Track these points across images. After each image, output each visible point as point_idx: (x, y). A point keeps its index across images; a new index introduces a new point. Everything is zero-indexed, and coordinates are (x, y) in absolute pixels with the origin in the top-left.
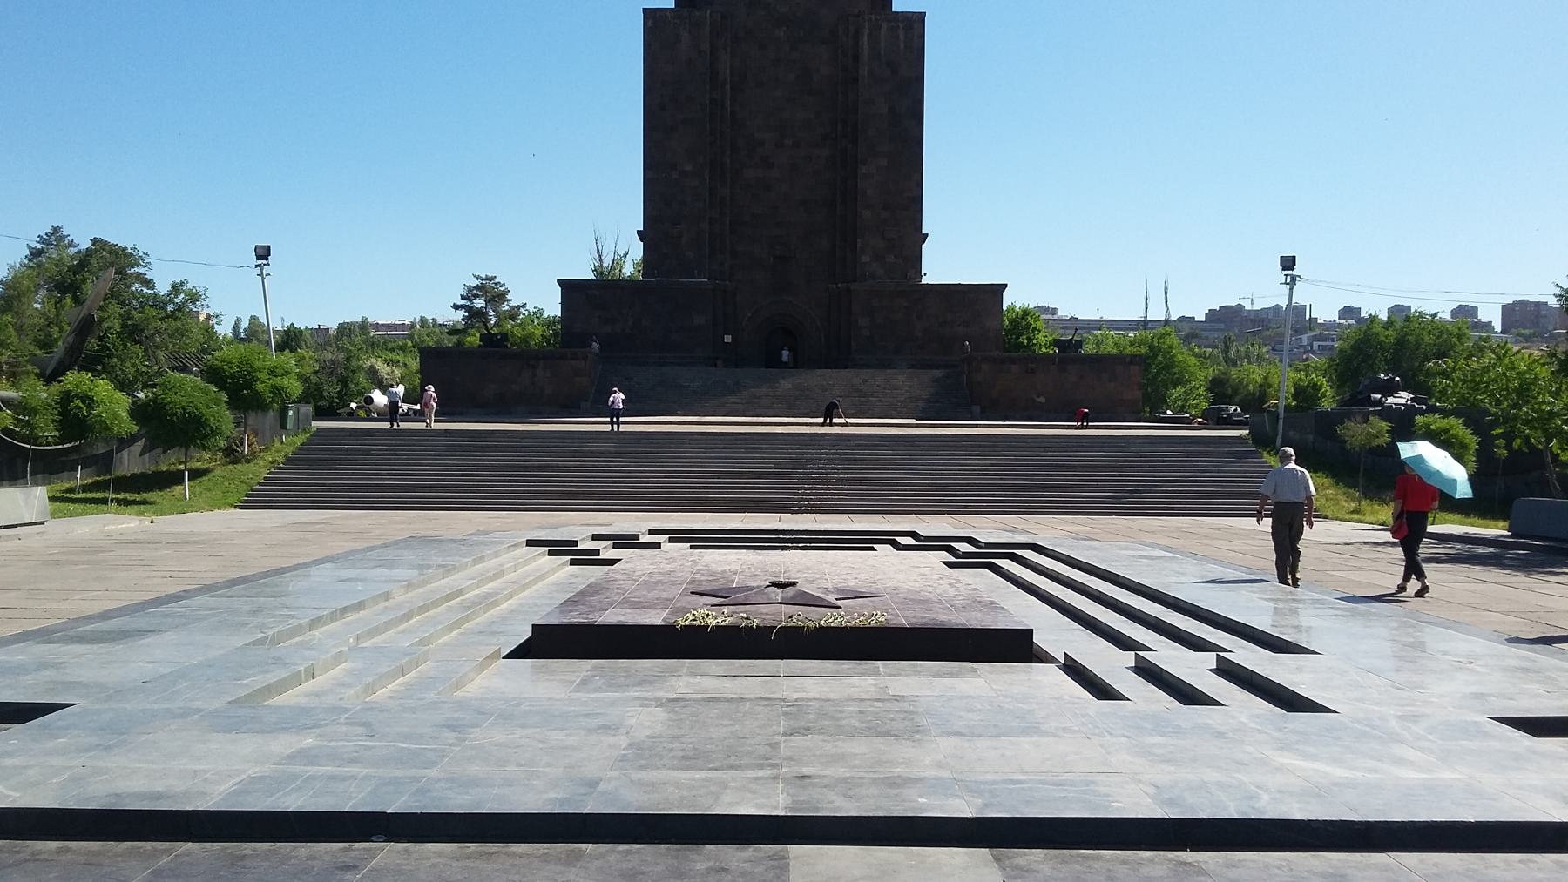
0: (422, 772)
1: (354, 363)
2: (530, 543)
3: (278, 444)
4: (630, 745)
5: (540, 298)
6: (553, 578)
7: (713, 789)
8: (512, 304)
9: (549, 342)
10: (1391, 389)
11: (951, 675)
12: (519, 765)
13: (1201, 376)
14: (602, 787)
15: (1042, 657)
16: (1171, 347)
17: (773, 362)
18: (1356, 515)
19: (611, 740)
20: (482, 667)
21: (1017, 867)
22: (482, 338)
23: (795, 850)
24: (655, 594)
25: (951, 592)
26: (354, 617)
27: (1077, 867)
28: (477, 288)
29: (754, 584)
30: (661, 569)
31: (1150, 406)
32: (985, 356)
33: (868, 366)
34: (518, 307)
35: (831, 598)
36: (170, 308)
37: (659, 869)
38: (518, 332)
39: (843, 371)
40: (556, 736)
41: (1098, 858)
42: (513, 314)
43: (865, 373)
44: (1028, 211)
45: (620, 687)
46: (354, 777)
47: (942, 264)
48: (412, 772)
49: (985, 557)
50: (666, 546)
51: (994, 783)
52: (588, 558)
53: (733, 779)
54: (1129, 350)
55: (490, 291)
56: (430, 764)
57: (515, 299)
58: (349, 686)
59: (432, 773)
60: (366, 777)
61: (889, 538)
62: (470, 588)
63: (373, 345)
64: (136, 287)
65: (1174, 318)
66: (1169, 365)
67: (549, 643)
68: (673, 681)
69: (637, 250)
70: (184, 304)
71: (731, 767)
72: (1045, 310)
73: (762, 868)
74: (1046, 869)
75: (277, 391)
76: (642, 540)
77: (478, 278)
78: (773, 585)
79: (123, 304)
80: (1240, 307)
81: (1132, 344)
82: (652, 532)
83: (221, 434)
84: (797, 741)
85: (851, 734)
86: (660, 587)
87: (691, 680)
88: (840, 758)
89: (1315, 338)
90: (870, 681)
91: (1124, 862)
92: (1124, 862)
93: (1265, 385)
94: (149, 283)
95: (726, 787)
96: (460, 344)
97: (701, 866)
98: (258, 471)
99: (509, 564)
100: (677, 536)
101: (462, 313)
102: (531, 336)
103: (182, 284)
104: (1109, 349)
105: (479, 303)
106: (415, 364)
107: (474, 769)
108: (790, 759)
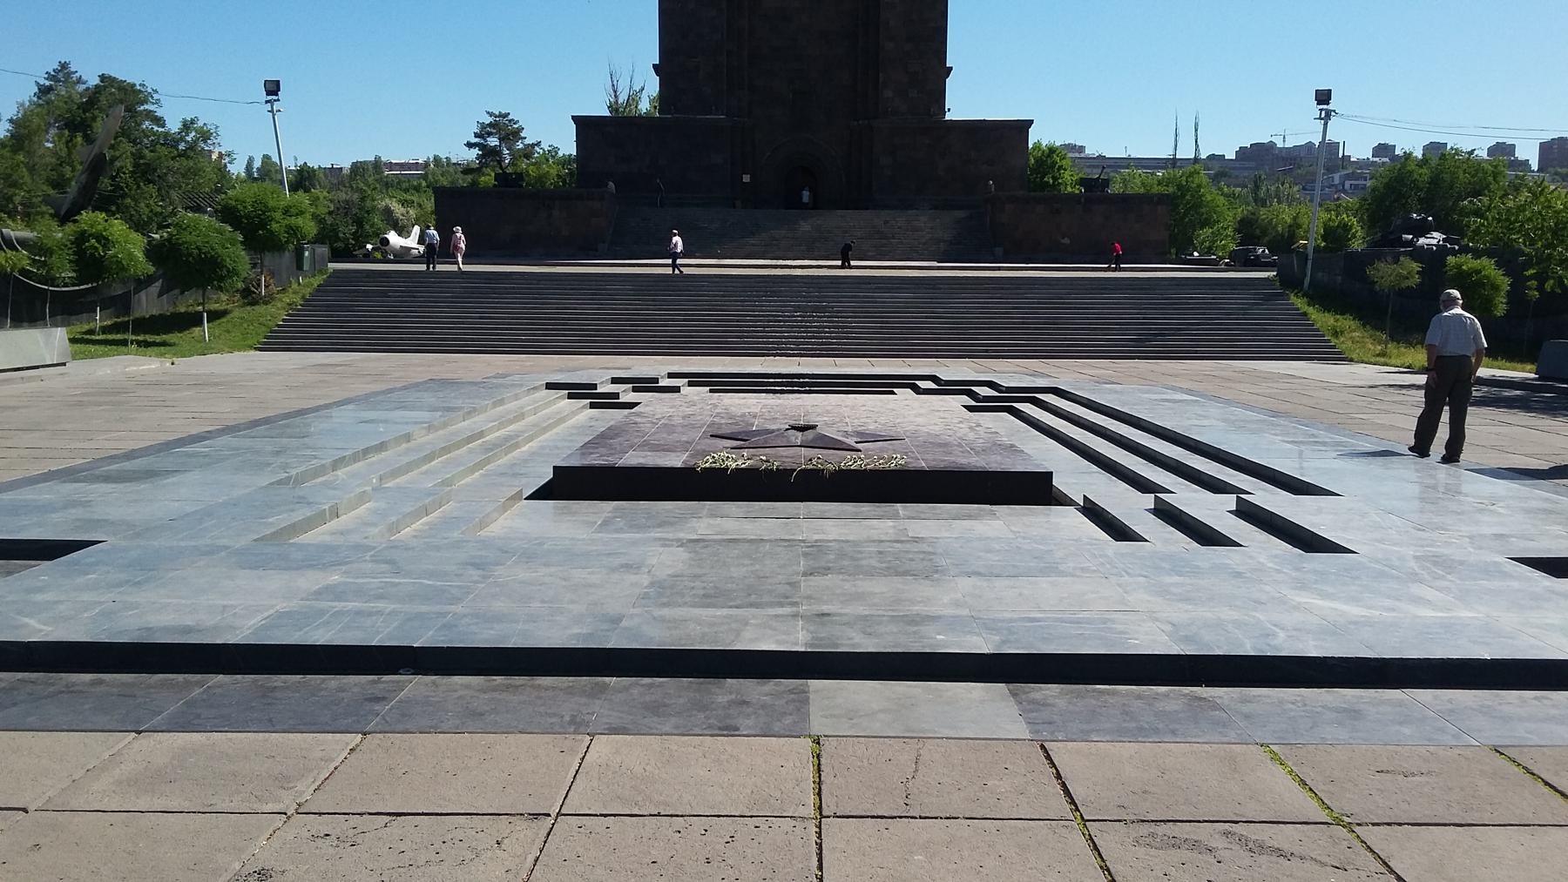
1: (368, 203)
2: (550, 386)
3: (295, 286)
4: (652, 584)
7: (734, 626)
8: (527, 142)
9: (564, 182)
10: (1423, 230)
11: (970, 517)
12: (543, 601)
13: (1230, 217)
14: (624, 623)
15: (1061, 500)
16: (1199, 186)
18: (1381, 358)
19: (633, 578)
21: (1033, 702)
25: (971, 436)
26: (375, 458)
28: (490, 125)
30: (682, 413)
31: (1176, 247)
34: (533, 145)
35: (851, 441)
36: (182, 146)
37: (681, 701)
38: (532, 171)
39: (867, 214)
41: (1114, 693)
42: (528, 152)
47: (969, 98)
48: (437, 608)
49: (1005, 401)
50: (686, 390)
51: (1011, 620)
53: (754, 617)
54: (1156, 189)
55: (503, 128)
56: (456, 600)
57: (530, 136)
58: (375, 525)
59: (458, 608)
61: (909, 382)
62: (491, 430)
63: (387, 185)
64: (147, 124)
65: (1203, 156)
66: (1198, 204)
67: (569, 485)
68: (694, 523)
69: (653, 86)
70: (195, 142)
71: (751, 605)
73: (782, 702)
74: (1061, 703)
75: (293, 231)
77: (491, 114)
78: (793, 428)
79: (134, 142)
80: (1272, 145)
82: (671, 375)
83: (237, 274)
84: (816, 581)
85: (871, 573)
87: (711, 521)
88: (859, 597)
89: (1348, 177)
90: (890, 523)
91: (1139, 697)
92: (1139, 697)
93: (1295, 225)
94: (159, 121)
95: (747, 624)
96: (474, 183)
97: (722, 699)
98: (276, 313)
99: (531, 408)
100: (696, 379)
101: (476, 151)
103: (192, 122)
104: (1136, 188)
105: (493, 141)
106: (430, 205)
107: (500, 605)
108: (809, 597)
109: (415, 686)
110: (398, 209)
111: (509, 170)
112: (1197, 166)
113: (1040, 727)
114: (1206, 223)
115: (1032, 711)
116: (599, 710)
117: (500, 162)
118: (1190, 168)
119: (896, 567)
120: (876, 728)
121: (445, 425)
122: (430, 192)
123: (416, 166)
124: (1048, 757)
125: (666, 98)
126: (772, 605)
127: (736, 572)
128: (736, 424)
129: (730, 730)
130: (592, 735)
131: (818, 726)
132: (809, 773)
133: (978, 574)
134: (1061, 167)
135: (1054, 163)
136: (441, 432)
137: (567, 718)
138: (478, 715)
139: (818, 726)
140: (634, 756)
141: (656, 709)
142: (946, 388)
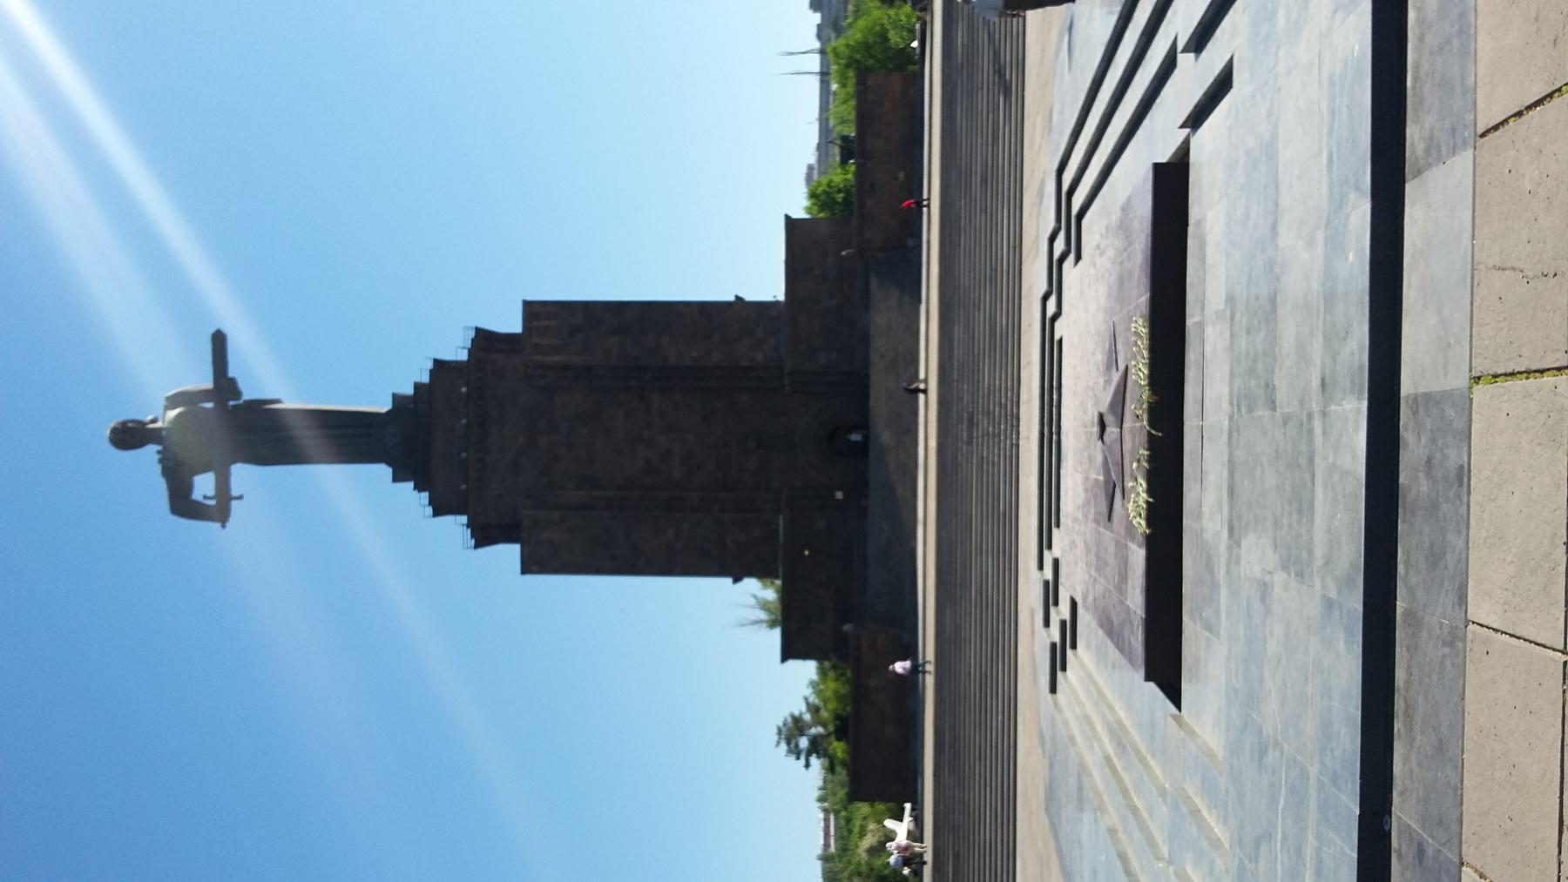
0: (1313, 781)
1: (864, 869)
2: (1053, 689)
4: (1285, 568)
5: (799, 684)
6: (1091, 666)
7: (1336, 478)
11: (1202, 246)
12: (1306, 682)
14: (1333, 594)
15: (1184, 152)
16: (848, 46)
17: (862, 450)
19: (1278, 590)
20: (1191, 732)
21: (1428, 151)
22: (839, 739)
23: (1406, 387)
24: (1111, 560)
25: (1111, 253)
26: (1135, 865)
27: (1426, 88)
28: (788, 744)
29: (1100, 458)
30: (1080, 552)
31: (909, 66)
32: (858, 234)
33: (867, 351)
34: (808, 704)
35: (1116, 377)
37: (1427, 530)
38: (832, 705)
40: (1273, 646)
41: (1417, 67)
42: (814, 709)
43: (874, 357)
44: (717, 213)
45: (1215, 587)
46: (1318, 851)
47: (766, 283)
48: (1313, 792)
49: (1070, 223)
50: (1057, 551)
51: (1331, 184)
52: (1070, 632)
53: (1325, 458)
54: (851, 89)
55: (792, 731)
56: (1304, 775)
57: (799, 708)
58: (1212, 863)
59: (1314, 770)
60: (1319, 838)
61: (1048, 324)
62: (1103, 749)
63: (845, 849)
65: (817, 45)
66: (866, 47)
67: (1164, 665)
68: (1208, 536)
69: (751, 585)
71: (1311, 461)
72: (809, 177)
73: (1428, 422)
74: (1429, 120)
76: (1046, 552)
77: (778, 743)
81: (844, 86)
82: (1041, 567)
84: (1281, 395)
85: (1273, 339)
86: (1102, 554)
87: (1206, 516)
88: (1302, 348)
90: (1209, 330)
91: (1421, 38)
92: (1421, 38)
95: (1334, 465)
96: (844, 764)
97: (1424, 486)
99: (1076, 712)
100: (1045, 541)
102: (836, 692)
104: (849, 110)
105: (804, 743)
106: (864, 808)
107: (1310, 727)
108: (1302, 402)
109: (1404, 813)
110: (869, 841)
111: (831, 728)
112: (829, 50)
113: (1459, 141)
114: (883, 36)
115: (1439, 152)
116: (1437, 617)
117: (822, 736)
118: (831, 57)
119: (1267, 312)
120: (1461, 317)
121: (1099, 796)
122: (850, 808)
123: (826, 820)
124: (1496, 128)
125: (763, 572)
126: (1311, 441)
127: (1271, 480)
128: (1096, 496)
129: (1463, 476)
130: (1467, 622)
131: (1457, 380)
132: (1517, 384)
133: (1274, 227)
134: (829, 185)
135: (825, 192)
136: (1105, 798)
137: (1447, 650)
138: (1441, 746)
139: (1457, 380)
140: (1490, 579)
141: (1435, 556)
142: (1055, 285)
